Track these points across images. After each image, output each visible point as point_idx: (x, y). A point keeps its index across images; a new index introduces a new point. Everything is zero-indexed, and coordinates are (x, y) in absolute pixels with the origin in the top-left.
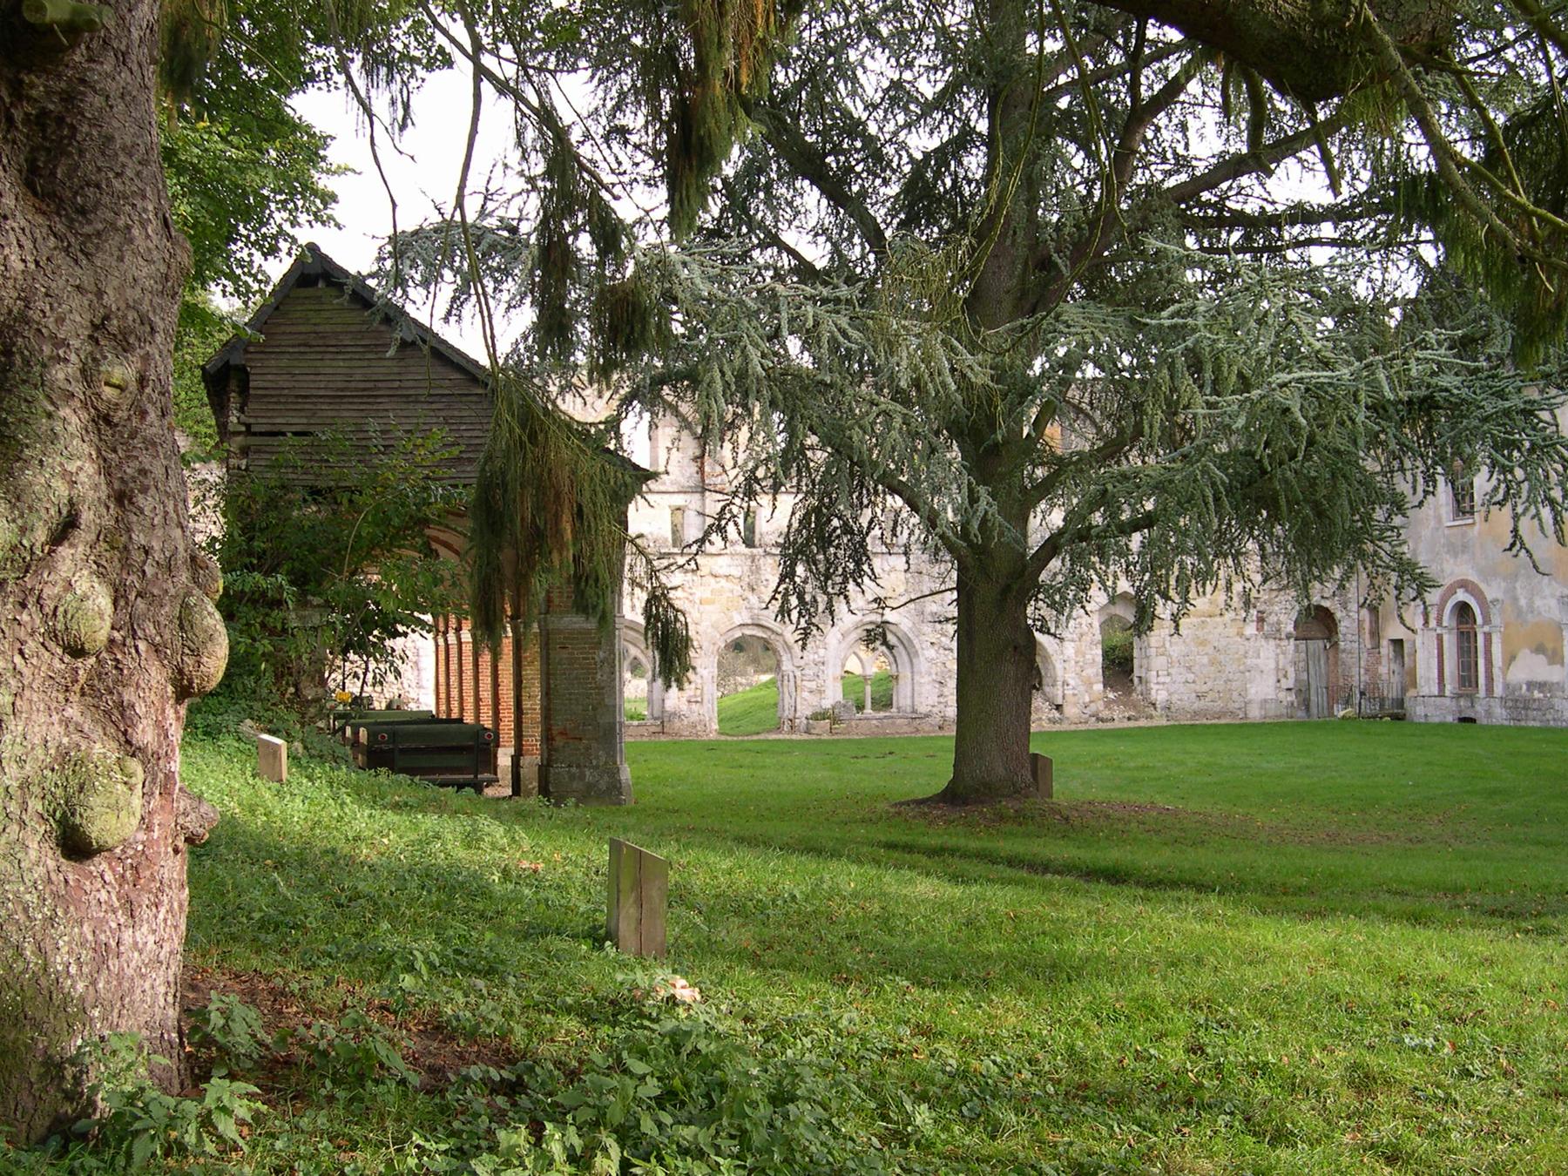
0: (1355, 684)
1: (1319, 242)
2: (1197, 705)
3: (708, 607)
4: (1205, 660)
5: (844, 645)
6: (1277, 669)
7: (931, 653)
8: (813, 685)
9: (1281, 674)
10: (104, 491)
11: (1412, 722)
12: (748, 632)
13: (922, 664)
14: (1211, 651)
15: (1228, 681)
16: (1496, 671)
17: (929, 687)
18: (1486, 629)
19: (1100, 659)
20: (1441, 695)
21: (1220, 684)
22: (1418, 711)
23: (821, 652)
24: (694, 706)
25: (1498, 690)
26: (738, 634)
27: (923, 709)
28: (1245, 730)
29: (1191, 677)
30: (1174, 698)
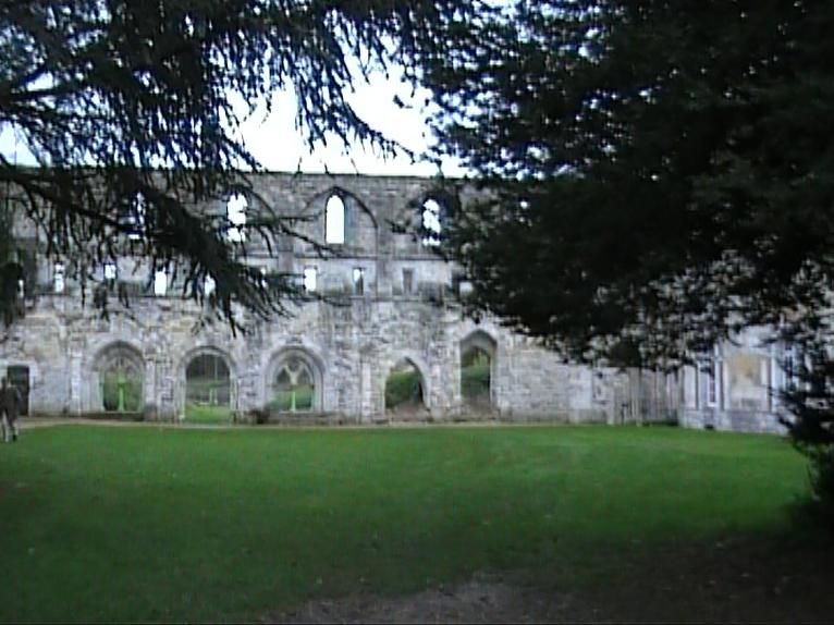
0: (669, 406)
1: (498, 44)
2: (532, 412)
3: (176, 334)
4: (538, 379)
5: (274, 363)
6: (593, 387)
7: (335, 370)
8: (250, 390)
9: (596, 390)
10: (91, 365)
11: (683, 429)
12: (207, 352)
13: (328, 378)
14: (542, 372)
15: (556, 395)
16: (726, 392)
17: (332, 394)
18: (720, 359)
19: (459, 377)
20: (697, 408)
21: (550, 398)
22: (685, 420)
23: (257, 367)
24: (166, 403)
25: (727, 406)
26: (199, 353)
27: (327, 409)
28: (567, 425)
29: (527, 391)
30: (515, 406)
